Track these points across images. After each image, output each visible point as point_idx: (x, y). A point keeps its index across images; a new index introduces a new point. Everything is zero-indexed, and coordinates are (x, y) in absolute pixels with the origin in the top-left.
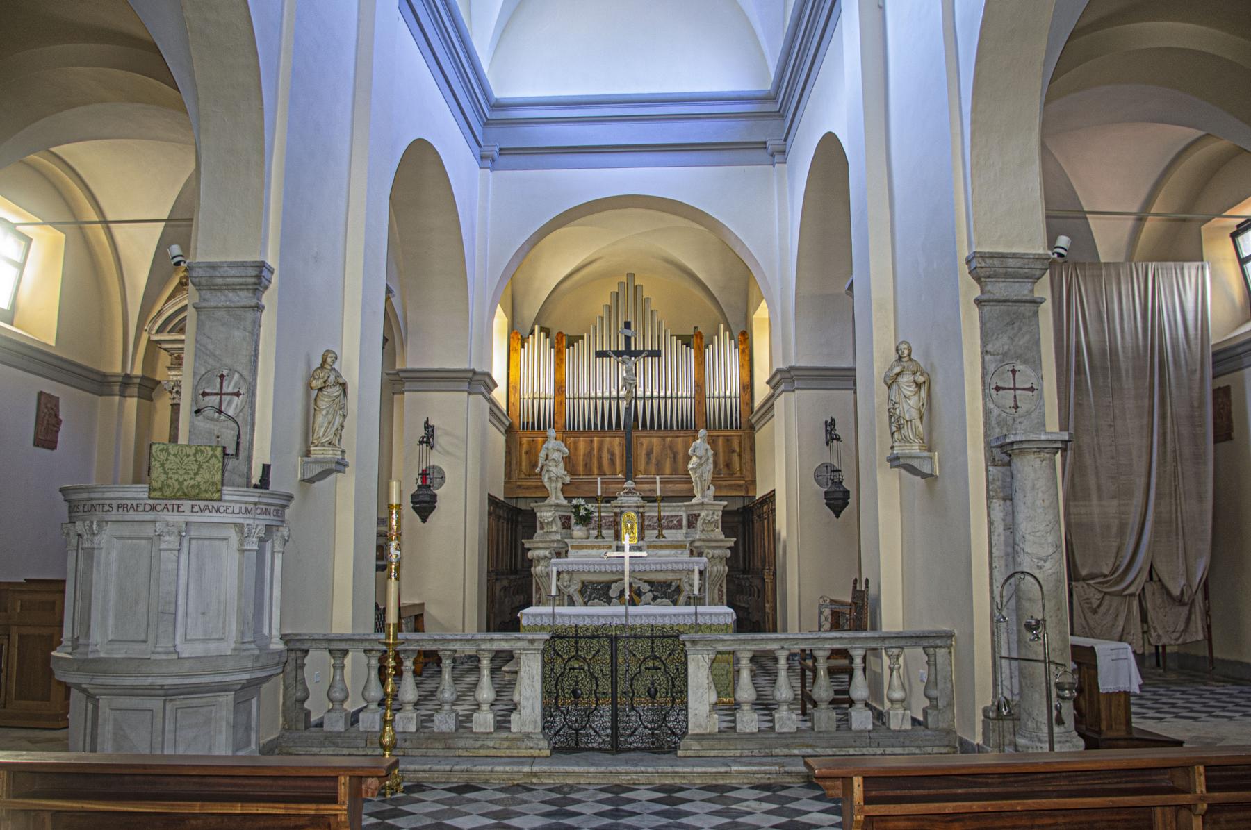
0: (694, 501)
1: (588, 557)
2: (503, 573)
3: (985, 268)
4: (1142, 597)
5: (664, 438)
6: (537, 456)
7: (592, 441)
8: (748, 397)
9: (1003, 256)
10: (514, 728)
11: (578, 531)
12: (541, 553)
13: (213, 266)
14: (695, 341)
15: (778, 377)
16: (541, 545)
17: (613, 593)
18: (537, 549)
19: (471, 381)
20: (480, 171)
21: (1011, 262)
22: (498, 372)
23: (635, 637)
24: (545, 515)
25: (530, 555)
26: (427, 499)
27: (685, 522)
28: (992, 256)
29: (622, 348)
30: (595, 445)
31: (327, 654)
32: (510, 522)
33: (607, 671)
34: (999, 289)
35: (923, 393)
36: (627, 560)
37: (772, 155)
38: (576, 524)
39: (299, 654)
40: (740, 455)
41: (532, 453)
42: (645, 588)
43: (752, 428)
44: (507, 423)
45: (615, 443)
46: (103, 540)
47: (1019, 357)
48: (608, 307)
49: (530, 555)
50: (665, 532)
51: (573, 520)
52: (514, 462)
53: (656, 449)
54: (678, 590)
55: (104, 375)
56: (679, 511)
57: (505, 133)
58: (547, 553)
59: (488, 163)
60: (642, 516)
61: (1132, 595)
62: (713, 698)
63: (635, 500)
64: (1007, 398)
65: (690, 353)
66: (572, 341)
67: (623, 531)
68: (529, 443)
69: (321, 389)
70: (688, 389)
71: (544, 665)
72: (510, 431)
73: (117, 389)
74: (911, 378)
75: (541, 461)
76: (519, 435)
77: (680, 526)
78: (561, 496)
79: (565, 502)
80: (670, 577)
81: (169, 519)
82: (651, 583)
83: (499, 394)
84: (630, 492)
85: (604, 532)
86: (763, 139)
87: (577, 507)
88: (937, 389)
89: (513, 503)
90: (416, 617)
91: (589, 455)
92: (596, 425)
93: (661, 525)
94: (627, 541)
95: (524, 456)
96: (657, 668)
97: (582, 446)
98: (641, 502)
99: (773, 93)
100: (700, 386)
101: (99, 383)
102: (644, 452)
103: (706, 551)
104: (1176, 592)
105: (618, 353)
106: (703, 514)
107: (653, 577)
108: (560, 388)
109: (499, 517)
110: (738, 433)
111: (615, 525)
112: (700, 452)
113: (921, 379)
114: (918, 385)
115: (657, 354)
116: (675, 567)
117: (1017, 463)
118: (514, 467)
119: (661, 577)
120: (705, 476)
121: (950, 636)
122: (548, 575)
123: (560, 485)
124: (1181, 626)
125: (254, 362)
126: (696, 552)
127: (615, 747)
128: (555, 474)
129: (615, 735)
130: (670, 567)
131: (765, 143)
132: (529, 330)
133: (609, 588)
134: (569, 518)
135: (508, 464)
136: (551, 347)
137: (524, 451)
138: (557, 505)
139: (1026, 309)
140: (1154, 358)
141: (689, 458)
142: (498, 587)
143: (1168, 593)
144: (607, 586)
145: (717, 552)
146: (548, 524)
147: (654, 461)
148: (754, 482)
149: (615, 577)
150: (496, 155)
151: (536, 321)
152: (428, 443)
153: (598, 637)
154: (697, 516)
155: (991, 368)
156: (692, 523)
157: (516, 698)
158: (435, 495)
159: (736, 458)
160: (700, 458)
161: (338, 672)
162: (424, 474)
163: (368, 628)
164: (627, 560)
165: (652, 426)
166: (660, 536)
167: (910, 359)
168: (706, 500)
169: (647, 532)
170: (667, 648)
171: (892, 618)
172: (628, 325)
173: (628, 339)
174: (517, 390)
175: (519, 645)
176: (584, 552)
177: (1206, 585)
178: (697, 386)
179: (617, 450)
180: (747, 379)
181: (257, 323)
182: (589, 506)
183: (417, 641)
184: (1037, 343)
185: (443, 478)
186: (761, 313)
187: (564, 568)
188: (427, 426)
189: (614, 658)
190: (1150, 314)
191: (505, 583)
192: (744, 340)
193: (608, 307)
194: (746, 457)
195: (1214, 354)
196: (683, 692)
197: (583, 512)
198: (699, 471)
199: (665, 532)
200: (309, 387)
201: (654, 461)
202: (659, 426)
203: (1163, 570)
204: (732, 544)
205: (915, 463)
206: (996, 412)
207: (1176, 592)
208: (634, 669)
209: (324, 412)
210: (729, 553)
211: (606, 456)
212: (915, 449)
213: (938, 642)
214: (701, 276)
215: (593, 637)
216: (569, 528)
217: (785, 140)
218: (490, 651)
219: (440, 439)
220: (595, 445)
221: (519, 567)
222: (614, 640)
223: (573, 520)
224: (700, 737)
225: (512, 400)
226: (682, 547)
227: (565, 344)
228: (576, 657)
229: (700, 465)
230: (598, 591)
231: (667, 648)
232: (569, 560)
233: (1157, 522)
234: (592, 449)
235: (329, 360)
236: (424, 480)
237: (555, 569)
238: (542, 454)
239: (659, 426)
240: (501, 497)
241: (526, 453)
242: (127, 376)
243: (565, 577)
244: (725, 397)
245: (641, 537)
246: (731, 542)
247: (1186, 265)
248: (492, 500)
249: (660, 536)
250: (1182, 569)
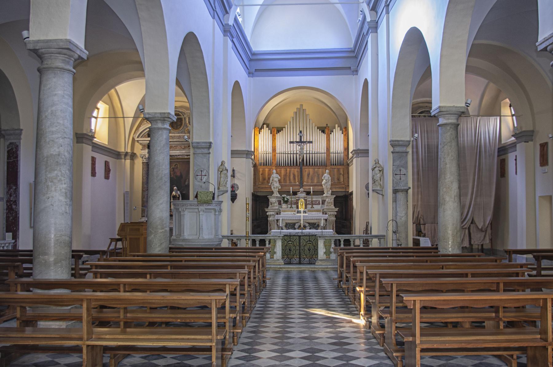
0: (324, 195)
1: (287, 214)
3: (394, 144)
4: (469, 229)
8: (346, 153)
9: (398, 141)
10: (275, 258)
11: (284, 206)
12: (272, 213)
13: (198, 143)
17: (296, 226)
18: (270, 212)
19: (247, 154)
21: (401, 143)
24: (272, 200)
28: (396, 141)
29: (298, 140)
32: (260, 201)
33: (298, 244)
34: (398, 149)
35: (381, 173)
42: (307, 225)
43: (348, 165)
45: (296, 171)
46: (186, 213)
47: (402, 166)
48: (293, 118)
49: (267, 214)
50: (314, 206)
51: (282, 202)
54: (318, 226)
55: (119, 152)
56: (319, 199)
57: (257, 64)
58: (273, 213)
60: (306, 200)
61: (465, 228)
62: (325, 251)
64: (398, 177)
65: (324, 136)
66: (279, 130)
68: (262, 171)
70: (323, 149)
73: (123, 157)
76: (260, 171)
77: (319, 204)
79: (279, 195)
80: (315, 221)
81: (160, 202)
82: (309, 223)
85: (293, 206)
87: (284, 198)
88: (384, 171)
93: (312, 203)
94: (302, 209)
98: (306, 196)
99: (353, 49)
100: (328, 149)
101: (117, 155)
104: (480, 227)
106: (327, 200)
107: (310, 221)
108: (274, 149)
111: (297, 203)
114: (380, 171)
115: (311, 142)
117: (397, 194)
121: (385, 236)
124: (482, 238)
125: (209, 167)
126: (324, 213)
127: (300, 263)
128: (276, 186)
129: (300, 261)
134: (280, 201)
139: (404, 154)
140: (478, 149)
141: (323, 180)
143: (478, 228)
144: (294, 224)
145: (332, 213)
147: (310, 178)
148: (348, 186)
154: (325, 201)
155: (395, 169)
156: (323, 203)
157: (275, 251)
158: (237, 194)
159: (342, 176)
163: (229, 235)
166: (312, 207)
168: (328, 195)
169: (308, 206)
170: (313, 239)
171: (374, 233)
173: (301, 137)
176: (286, 213)
177: (491, 224)
179: (296, 173)
180: (346, 146)
181: (209, 157)
184: (407, 163)
185: (238, 188)
189: (300, 241)
190: (477, 135)
192: (345, 130)
193: (293, 118)
194: (346, 176)
195: (498, 149)
196: (317, 250)
197: (286, 199)
199: (314, 206)
200: (218, 170)
201: (310, 178)
203: (476, 220)
205: (378, 192)
206: (395, 180)
207: (480, 227)
208: (305, 244)
210: (336, 213)
212: (378, 188)
214: (329, 105)
219: (237, 175)
220: (288, 171)
222: (300, 236)
223: (282, 202)
224: (321, 260)
229: (326, 183)
231: (313, 239)
233: (475, 205)
236: (233, 189)
242: (127, 153)
245: (306, 208)
246: (337, 209)
247: (491, 118)
249: (312, 207)
250: (482, 220)
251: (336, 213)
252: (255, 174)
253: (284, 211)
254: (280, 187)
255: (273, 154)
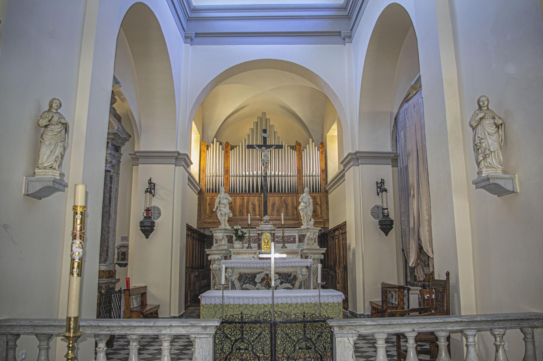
0: (302, 227)
1: (243, 259)
2: (195, 268)
5: (281, 197)
6: (214, 202)
7: (243, 199)
8: (324, 176)
11: (237, 245)
12: (216, 257)
14: (298, 148)
15: (349, 158)
16: (216, 252)
17: (258, 279)
18: (214, 254)
20: (184, 45)
22: (195, 157)
23: (291, 322)
24: (218, 235)
25: (209, 258)
26: (149, 224)
27: (297, 239)
29: (260, 142)
30: (245, 200)
31: (35, 337)
32: (198, 241)
36: (273, 261)
37: (344, 39)
38: (236, 240)
39: (10, 337)
40: (321, 206)
41: (212, 204)
43: (327, 192)
44: (199, 189)
48: (253, 130)
49: (209, 258)
50: (286, 245)
51: (234, 238)
52: (202, 209)
53: (277, 203)
56: (295, 233)
59: (189, 41)
60: (273, 235)
63: (270, 226)
65: (295, 154)
66: (233, 148)
67: (263, 244)
68: (210, 199)
69: (46, 126)
71: (215, 344)
72: (200, 193)
74: (492, 121)
75: (216, 204)
76: (205, 196)
77: (294, 242)
78: (228, 225)
80: (290, 270)
83: (194, 169)
84: (267, 222)
85: (252, 245)
86: (339, 30)
87: (237, 230)
89: (202, 231)
90: (142, 294)
91: (242, 205)
92: (245, 190)
95: (208, 206)
96: (308, 348)
97: (238, 200)
100: (300, 171)
102: (271, 204)
103: (310, 255)
105: (260, 147)
106: (308, 234)
108: (227, 171)
109: (193, 238)
110: (322, 192)
112: (305, 200)
113: (500, 122)
114: (497, 127)
116: (293, 264)
118: (202, 212)
119: (285, 270)
120: (308, 213)
122: (220, 269)
123: (227, 218)
128: (224, 212)
130: (291, 265)
131: (340, 32)
132: (211, 141)
133: (255, 277)
134: (232, 237)
135: (199, 210)
136: (222, 150)
137: (207, 203)
138: (225, 229)
141: (299, 203)
142: (193, 276)
144: (254, 276)
145: (317, 256)
146: (220, 240)
147: (276, 209)
149: (259, 271)
150: (193, 36)
151: (216, 136)
152: (151, 192)
153: (260, 322)
154: (304, 236)
158: (154, 222)
159: (318, 207)
160: (306, 203)
161: (43, 352)
162: (148, 210)
164: (273, 261)
165: (274, 190)
167: (488, 109)
168: (309, 227)
171: (468, 298)
172: (265, 131)
173: (265, 139)
174: (204, 171)
175: (194, 330)
178: (298, 170)
179: (257, 203)
180: (324, 167)
182: (244, 230)
183: (108, 327)
185: (160, 213)
186: (333, 132)
187: (229, 265)
188: (150, 182)
189: (273, 339)
191: (197, 273)
192: (322, 146)
193: (252, 130)
194: (324, 207)
197: (240, 233)
198: (305, 210)
201: (276, 209)
202: (279, 191)
204: (324, 252)
209: (47, 143)
210: (322, 257)
211: (251, 206)
213: (536, 323)
215: (255, 322)
216: (232, 242)
217: (351, 30)
218: (169, 335)
219: (159, 191)
220: (245, 200)
221: (205, 265)
222: (273, 325)
223: (234, 238)
225: (201, 177)
226: (296, 253)
227: (229, 148)
228: (242, 339)
229: (306, 207)
230: (248, 280)
232: (232, 260)
234: (244, 202)
235: (54, 105)
237: (224, 266)
238: (217, 201)
239: (279, 191)
240: (195, 227)
241: (209, 204)
243: (230, 270)
244: (313, 176)
246: (324, 250)
248: (189, 228)
251: (322, 257)
252: (199, 204)
253: (238, 254)
254: (231, 215)
255: (226, 177)
